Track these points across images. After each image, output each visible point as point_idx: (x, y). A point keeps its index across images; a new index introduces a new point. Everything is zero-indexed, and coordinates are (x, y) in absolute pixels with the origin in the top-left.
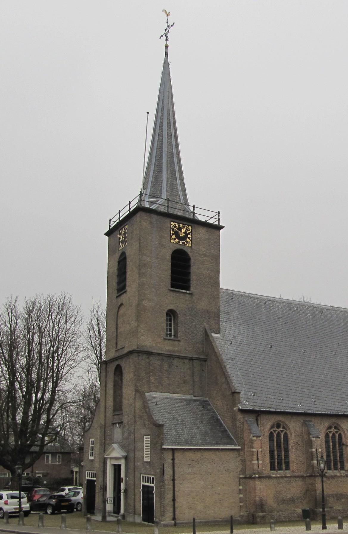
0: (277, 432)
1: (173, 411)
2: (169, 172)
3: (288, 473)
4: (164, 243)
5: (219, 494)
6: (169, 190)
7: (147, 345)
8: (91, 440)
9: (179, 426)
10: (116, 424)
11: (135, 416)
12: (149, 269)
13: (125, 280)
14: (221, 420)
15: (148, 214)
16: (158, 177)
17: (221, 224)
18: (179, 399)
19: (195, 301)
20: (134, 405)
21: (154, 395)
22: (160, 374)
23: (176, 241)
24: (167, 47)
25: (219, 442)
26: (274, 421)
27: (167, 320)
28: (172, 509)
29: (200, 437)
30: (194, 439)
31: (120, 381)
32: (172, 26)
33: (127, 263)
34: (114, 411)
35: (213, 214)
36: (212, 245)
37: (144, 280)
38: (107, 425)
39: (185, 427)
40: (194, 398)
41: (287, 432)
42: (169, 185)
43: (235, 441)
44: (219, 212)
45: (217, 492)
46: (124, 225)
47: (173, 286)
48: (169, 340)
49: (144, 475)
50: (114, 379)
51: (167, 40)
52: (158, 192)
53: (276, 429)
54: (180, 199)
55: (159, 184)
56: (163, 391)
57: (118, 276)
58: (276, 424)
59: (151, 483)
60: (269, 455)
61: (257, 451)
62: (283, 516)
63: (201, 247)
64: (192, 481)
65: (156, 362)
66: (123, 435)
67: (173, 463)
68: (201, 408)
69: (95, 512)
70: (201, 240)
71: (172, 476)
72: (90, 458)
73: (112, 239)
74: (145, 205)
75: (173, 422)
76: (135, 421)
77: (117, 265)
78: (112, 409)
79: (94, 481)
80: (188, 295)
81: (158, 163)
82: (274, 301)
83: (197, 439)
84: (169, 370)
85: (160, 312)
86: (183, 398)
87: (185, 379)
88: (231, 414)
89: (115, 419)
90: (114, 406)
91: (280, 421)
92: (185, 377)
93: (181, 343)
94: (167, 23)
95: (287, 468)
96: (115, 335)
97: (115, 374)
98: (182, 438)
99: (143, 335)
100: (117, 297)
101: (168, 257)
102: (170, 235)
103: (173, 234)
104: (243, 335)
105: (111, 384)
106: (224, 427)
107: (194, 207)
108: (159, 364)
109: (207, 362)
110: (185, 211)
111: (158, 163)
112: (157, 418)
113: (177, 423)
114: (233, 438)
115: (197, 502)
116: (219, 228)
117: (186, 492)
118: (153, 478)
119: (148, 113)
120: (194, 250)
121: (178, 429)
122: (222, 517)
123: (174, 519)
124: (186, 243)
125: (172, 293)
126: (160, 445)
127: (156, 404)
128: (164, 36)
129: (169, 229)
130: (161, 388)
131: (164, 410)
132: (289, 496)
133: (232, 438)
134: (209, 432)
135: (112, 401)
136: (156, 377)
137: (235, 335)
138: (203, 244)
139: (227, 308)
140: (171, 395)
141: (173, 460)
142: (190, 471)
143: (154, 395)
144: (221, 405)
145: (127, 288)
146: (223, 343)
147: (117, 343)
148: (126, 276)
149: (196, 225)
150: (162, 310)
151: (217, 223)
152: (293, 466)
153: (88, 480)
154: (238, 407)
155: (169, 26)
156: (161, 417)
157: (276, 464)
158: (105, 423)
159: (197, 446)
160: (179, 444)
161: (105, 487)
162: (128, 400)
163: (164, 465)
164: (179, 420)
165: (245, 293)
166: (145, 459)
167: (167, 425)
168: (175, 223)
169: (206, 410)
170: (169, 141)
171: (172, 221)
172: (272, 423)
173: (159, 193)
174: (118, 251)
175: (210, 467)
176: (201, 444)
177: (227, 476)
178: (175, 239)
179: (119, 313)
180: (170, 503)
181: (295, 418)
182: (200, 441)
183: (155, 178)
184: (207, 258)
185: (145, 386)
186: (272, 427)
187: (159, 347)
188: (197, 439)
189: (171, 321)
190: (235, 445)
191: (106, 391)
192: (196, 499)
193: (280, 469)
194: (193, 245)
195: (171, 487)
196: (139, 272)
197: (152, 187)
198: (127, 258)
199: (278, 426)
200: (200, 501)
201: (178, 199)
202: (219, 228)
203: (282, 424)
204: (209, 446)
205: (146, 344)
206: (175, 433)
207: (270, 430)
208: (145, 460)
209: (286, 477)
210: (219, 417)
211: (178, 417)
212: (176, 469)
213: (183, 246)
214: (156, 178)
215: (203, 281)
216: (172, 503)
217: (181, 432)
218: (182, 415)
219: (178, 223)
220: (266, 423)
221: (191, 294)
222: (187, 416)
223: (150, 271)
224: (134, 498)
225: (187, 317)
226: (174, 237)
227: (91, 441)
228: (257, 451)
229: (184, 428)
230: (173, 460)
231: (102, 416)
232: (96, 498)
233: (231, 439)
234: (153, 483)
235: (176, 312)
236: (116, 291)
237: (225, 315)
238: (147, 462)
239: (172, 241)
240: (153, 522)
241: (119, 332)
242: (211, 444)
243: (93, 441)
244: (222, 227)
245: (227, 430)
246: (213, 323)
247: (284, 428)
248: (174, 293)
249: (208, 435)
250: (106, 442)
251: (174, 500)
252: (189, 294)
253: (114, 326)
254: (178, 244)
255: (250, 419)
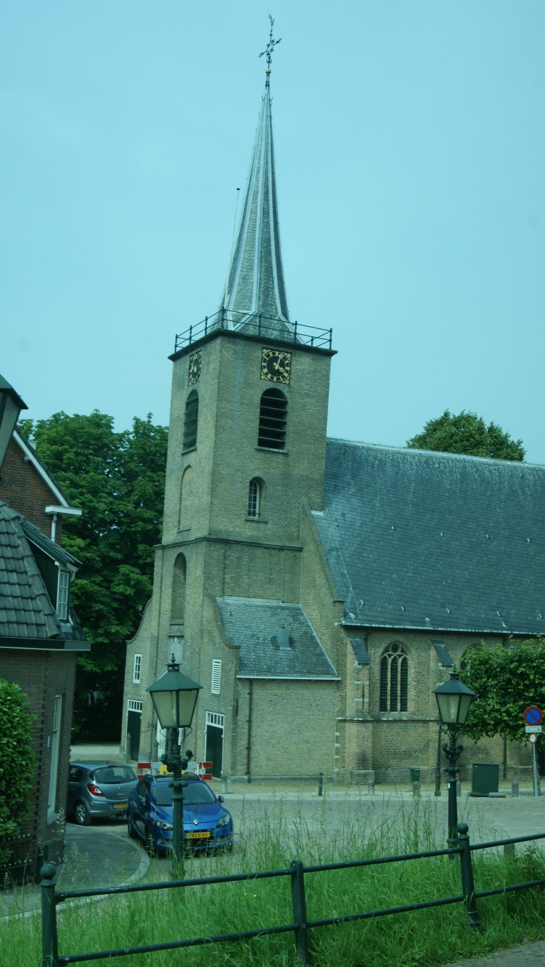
0: (393, 657)
1: (253, 625)
2: (263, 269)
3: (405, 716)
4: (252, 381)
5: (308, 742)
6: (262, 296)
7: (222, 529)
8: (136, 655)
9: (259, 646)
10: (173, 637)
11: (202, 631)
12: (229, 420)
13: (195, 422)
14: (317, 639)
15: (231, 340)
16: (247, 277)
17: (333, 349)
18: (262, 606)
19: (291, 464)
20: (201, 614)
21: (229, 601)
22: (238, 570)
23: (268, 376)
24: (268, 73)
25: (313, 671)
26: (390, 642)
27: (250, 492)
28: (245, 760)
29: (287, 663)
30: (279, 665)
31: (182, 577)
32: (278, 42)
33: (200, 408)
34: (172, 618)
35: (320, 333)
36: (319, 379)
37: (223, 436)
38: (160, 637)
39: (267, 648)
40: (281, 604)
41: (407, 657)
42: (262, 290)
43: (334, 669)
44: (331, 329)
45: (305, 739)
46: (196, 351)
47: (261, 443)
48: (252, 521)
49: (211, 713)
50: (174, 573)
51: (269, 62)
52: (247, 300)
53: (392, 653)
54: (276, 309)
55: (248, 288)
56: (240, 595)
57: (185, 424)
58: (391, 646)
59: (219, 724)
60: (379, 689)
61: (363, 686)
62: (394, 775)
63: (302, 383)
64: (274, 723)
65: (233, 554)
66: (184, 653)
67: (251, 699)
68: (291, 619)
69: (139, 757)
70: (304, 373)
71: (248, 715)
72: (134, 682)
73: (178, 366)
74: (227, 326)
75: (252, 640)
76: (202, 637)
77: (185, 408)
78: (170, 615)
79: (139, 714)
80: (281, 457)
81: (249, 255)
82: (406, 455)
83: (282, 665)
84: (250, 565)
85: (242, 482)
86: (267, 604)
87: (271, 577)
88: (331, 630)
89: (172, 631)
90: (172, 611)
91: (397, 641)
92: (271, 574)
93: (269, 526)
94: (271, 35)
95: (404, 708)
96: (177, 509)
97: (175, 565)
98: (264, 664)
99: (217, 516)
100: (183, 455)
101: (257, 400)
102: (260, 369)
103: (264, 367)
104: (356, 511)
105: (170, 579)
106: (321, 648)
107: (296, 324)
108: (237, 556)
109: (302, 553)
110: (284, 330)
111: (249, 255)
112: (231, 635)
113: (258, 642)
114: (331, 664)
115: (278, 752)
116: (330, 353)
117: (264, 738)
118: (222, 717)
119: (238, 189)
120: (292, 389)
121: (258, 652)
122: (310, 774)
123: (248, 773)
124: (282, 379)
125: (260, 454)
126: (234, 673)
127: (231, 615)
128: (265, 54)
129: (260, 359)
130: (237, 590)
131: (241, 624)
132: (404, 748)
133: (330, 665)
134: (300, 656)
135: (170, 604)
136: (231, 575)
137: (344, 512)
138: (307, 379)
139: (335, 469)
140: (251, 599)
141: (251, 694)
142: (271, 709)
143: (229, 600)
144: (319, 617)
145: (198, 445)
146: (326, 525)
147: (179, 521)
148: (197, 427)
149: (297, 352)
150: (244, 479)
151: (326, 346)
152: (411, 705)
153: (130, 712)
154: (341, 621)
155: (273, 41)
156: (236, 633)
157: (389, 703)
158: (158, 635)
159: (283, 676)
160: (259, 672)
161: (154, 724)
162: (193, 606)
163: (237, 701)
164: (261, 639)
165: (364, 443)
166: (212, 690)
167: (244, 645)
168: (268, 351)
169: (297, 623)
170: (265, 220)
171: (263, 348)
172: (387, 645)
173: (248, 302)
174: (187, 386)
175: (297, 705)
176: (287, 674)
177: (321, 718)
178: (267, 374)
179: (185, 477)
180: (243, 752)
181: (419, 637)
182: (287, 669)
183: (243, 279)
184: (309, 400)
185: (217, 588)
186: (386, 650)
187: (237, 532)
188: (282, 665)
189: (255, 493)
190: (333, 675)
191: (161, 588)
192: (276, 748)
193: (394, 709)
194: (291, 381)
195: (246, 731)
196: (216, 425)
197: (239, 292)
198: (200, 400)
199: (395, 649)
200: (283, 751)
201: (274, 311)
202: (330, 353)
203: (400, 645)
204: (297, 676)
205: (220, 528)
206: (254, 657)
207: (383, 654)
208: (213, 692)
209: (401, 721)
210: (315, 634)
211: (259, 633)
212: (254, 706)
213: (279, 384)
214: (243, 279)
215: (303, 434)
216: (245, 752)
217: (262, 655)
218: (264, 631)
219: (272, 350)
220: (377, 645)
221: (286, 455)
222: (271, 632)
223: (231, 423)
224: (196, 743)
225: (278, 488)
226: (265, 370)
227: (137, 657)
228: (363, 686)
229: (266, 650)
230: (251, 694)
231: (154, 624)
232: (141, 739)
233: (329, 666)
234: (222, 725)
235: (263, 481)
236: (182, 446)
237: (333, 480)
238: (215, 695)
239: (263, 377)
240: (219, 776)
241: (182, 506)
242: (301, 673)
243: (140, 658)
244: (335, 352)
245: (324, 653)
246: (314, 495)
247: (403, 651)
248: (263, 454)
249: (298, 660)
250: (159, 661)
251: (249, 748)
252: (282, 453)
253: (177, 496)
254: (270, 380)
255: (357, 639)
